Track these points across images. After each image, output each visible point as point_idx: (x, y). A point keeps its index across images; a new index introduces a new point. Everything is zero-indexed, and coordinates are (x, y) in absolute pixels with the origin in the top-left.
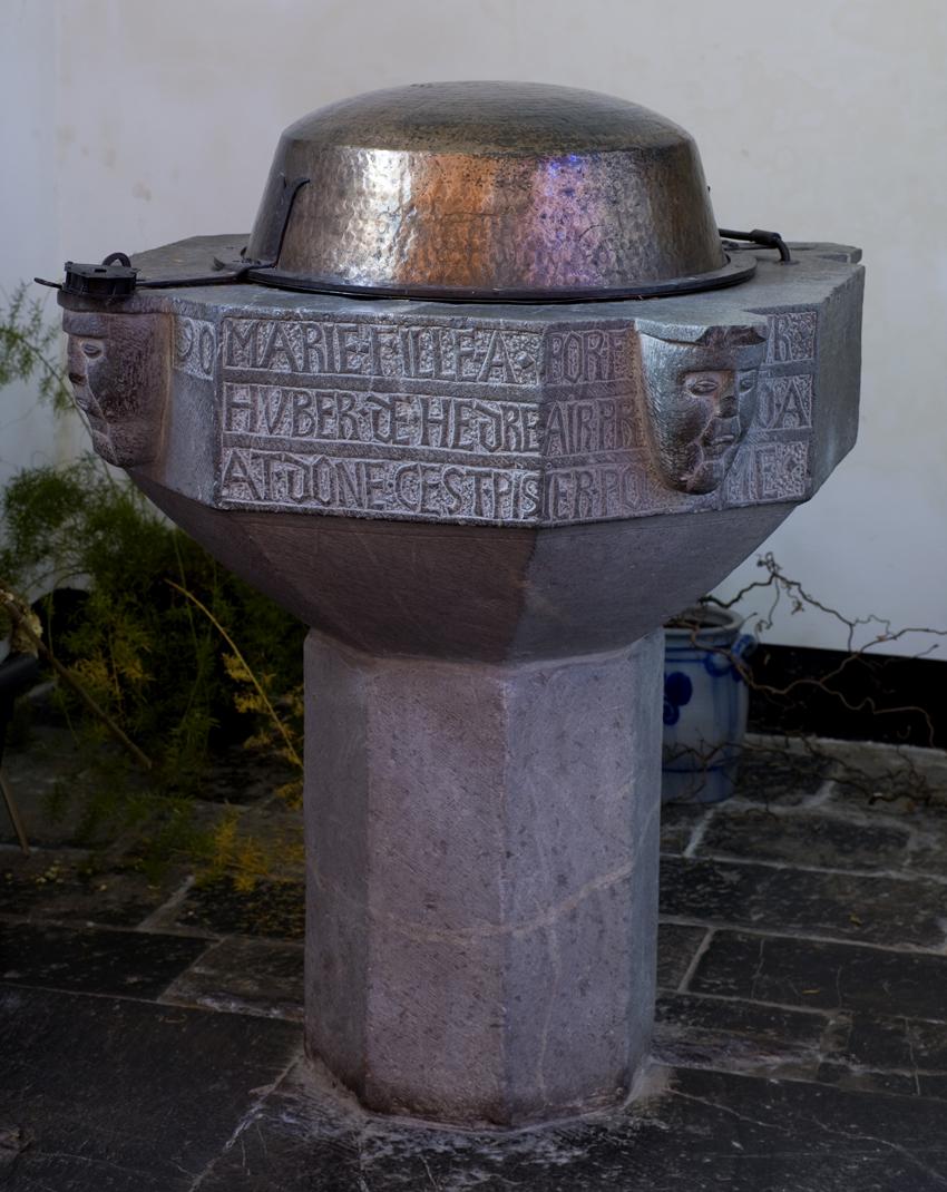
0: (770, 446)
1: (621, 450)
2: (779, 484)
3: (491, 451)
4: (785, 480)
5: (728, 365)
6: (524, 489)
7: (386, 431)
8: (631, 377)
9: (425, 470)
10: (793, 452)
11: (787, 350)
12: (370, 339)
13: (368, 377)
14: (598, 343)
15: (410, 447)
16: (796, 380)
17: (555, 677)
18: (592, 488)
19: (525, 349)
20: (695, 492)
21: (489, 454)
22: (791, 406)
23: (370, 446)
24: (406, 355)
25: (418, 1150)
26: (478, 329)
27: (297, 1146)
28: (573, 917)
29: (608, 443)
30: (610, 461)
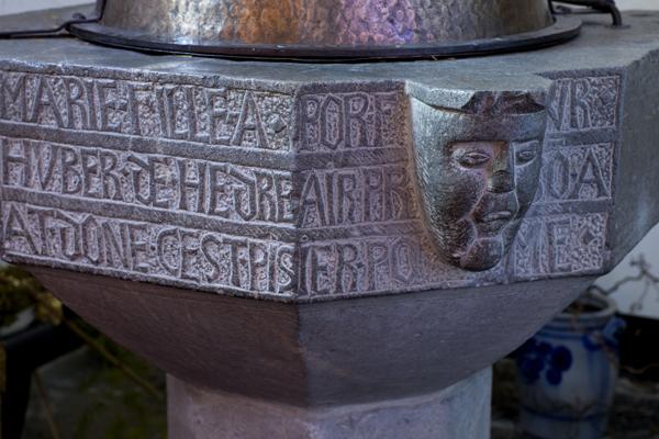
0: (564, 218)
1: (391, 221)
2: (573, 257)
3: (247, 219)
4: (580, 253)
5: (499, 136)
7: (146, 193)
8: (402, 144)
9: (184, 235)
10: (590, 224)
11: (586, 117)
12: (128, 96)
13: (127, 136)
14: (362, 106)
15: (169, 210)
16: (595, 149)
17: (364, 420)
19: (276, 112)
20: (470, 268)
21: (244, 222)
22: (589, 175)
23: (132, 207)
24: (162, 113)
26: (229, 89)
29: (374, 215)
30: (374, 233)
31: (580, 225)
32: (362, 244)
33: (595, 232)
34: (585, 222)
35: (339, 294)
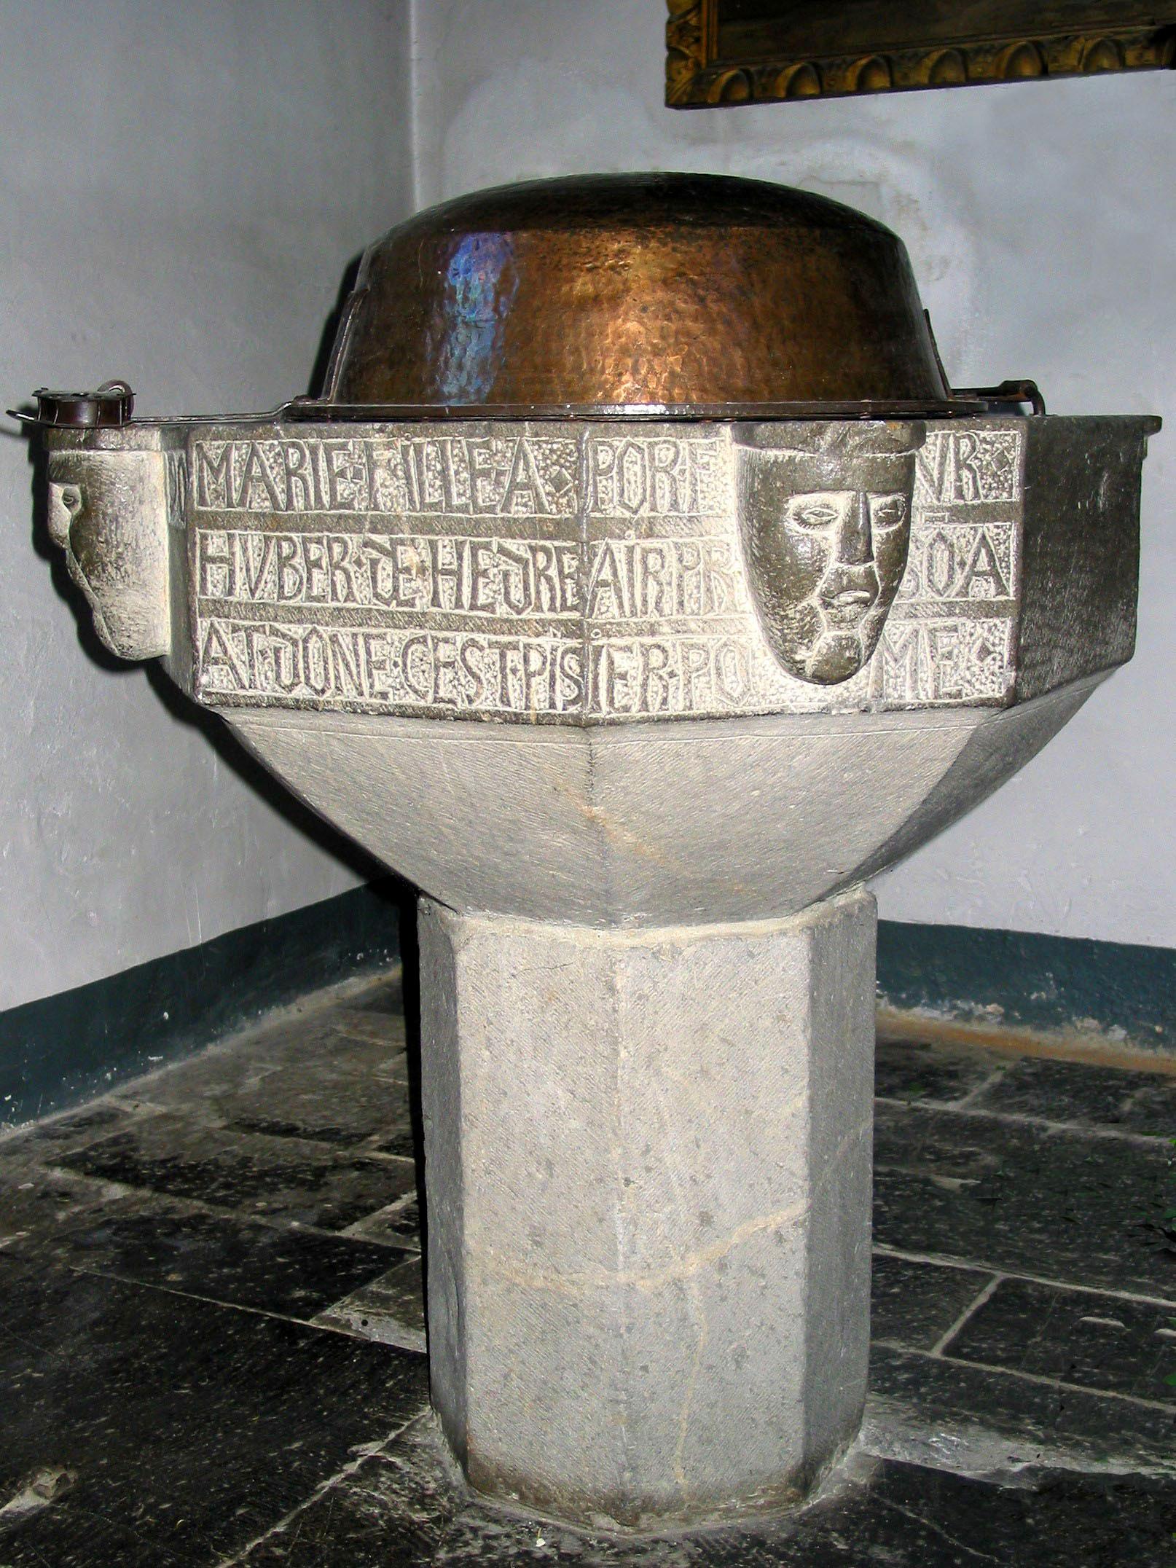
6: (562, 667)
7: (385, 586)
9: (436, 641)
10: (985, 634)
12: (364, 460)
16: (989, 529)
18: (668, 669)
20: (821, 679)
22: (983, 564)
25: (513, 1551)
27: (364, 1531)
28: (722, 1267)
29: (690, 605)
31: (971, 635)
32: (674, 646)
33: (994, 645)
34: (979, 630)
35: (645, 714)
